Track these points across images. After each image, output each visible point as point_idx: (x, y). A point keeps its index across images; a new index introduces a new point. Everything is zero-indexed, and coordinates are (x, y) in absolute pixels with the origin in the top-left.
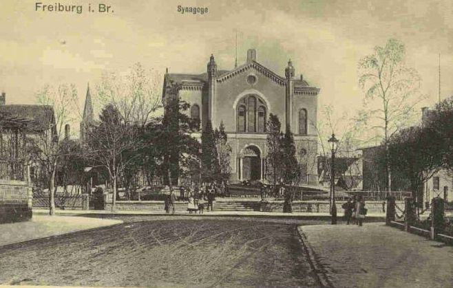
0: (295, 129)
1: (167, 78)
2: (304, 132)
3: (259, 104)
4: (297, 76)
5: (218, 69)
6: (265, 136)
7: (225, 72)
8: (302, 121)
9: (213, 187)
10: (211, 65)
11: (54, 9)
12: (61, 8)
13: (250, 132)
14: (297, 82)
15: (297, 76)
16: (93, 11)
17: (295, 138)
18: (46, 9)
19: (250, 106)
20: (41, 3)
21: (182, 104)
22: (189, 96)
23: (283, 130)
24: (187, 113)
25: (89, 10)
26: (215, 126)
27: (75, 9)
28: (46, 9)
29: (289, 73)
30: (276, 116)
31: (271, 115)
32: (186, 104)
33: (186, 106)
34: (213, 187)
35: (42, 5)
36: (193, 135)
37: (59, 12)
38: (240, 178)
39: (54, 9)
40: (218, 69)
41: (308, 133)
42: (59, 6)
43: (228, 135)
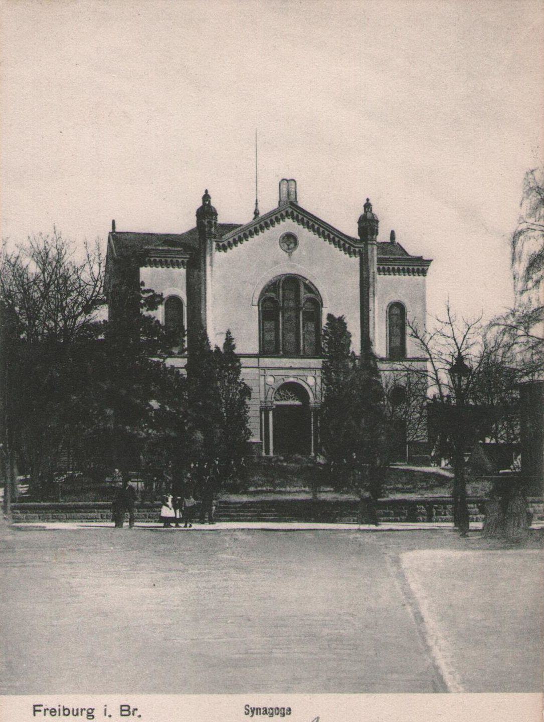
0: (380, 348)
1: (117, 239)
2: (397, 352)
3: (304, 295)
4: (383, 236)
5: (222, 219)
6: (317, 363)
7: (236, 226)
8: (397, 330)
9: (211, 471)
10: (206, 212)
11: (57, 713)
12: (66, 712)
13: (287, 355)
14: (382, 246)
15: (383, 236)
16: (110, 716)
17: (381, 366)
18: (48, 712)
19: (287, 306)
20: (42, 706)
21: (146, 295)
22: (164, 280)
23: (356, 346)
24: (159, 314)
25: (106, 715)
26: (216, 340)
27: (85, 713)
28: (48, 712)
29: (368, 223)
30: (341, 319)
31: (330, 317)
32: (155, 296)
33: (154, 301)
34: (211, 471)
35: (42, 708)
36: (170, 362)
37: (65, 717)
38: (267, 452)
39: (57, 713)
40: (222, 219)
41: (409, 355)
42: (64, 709)
43: (242, 360)
